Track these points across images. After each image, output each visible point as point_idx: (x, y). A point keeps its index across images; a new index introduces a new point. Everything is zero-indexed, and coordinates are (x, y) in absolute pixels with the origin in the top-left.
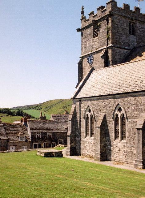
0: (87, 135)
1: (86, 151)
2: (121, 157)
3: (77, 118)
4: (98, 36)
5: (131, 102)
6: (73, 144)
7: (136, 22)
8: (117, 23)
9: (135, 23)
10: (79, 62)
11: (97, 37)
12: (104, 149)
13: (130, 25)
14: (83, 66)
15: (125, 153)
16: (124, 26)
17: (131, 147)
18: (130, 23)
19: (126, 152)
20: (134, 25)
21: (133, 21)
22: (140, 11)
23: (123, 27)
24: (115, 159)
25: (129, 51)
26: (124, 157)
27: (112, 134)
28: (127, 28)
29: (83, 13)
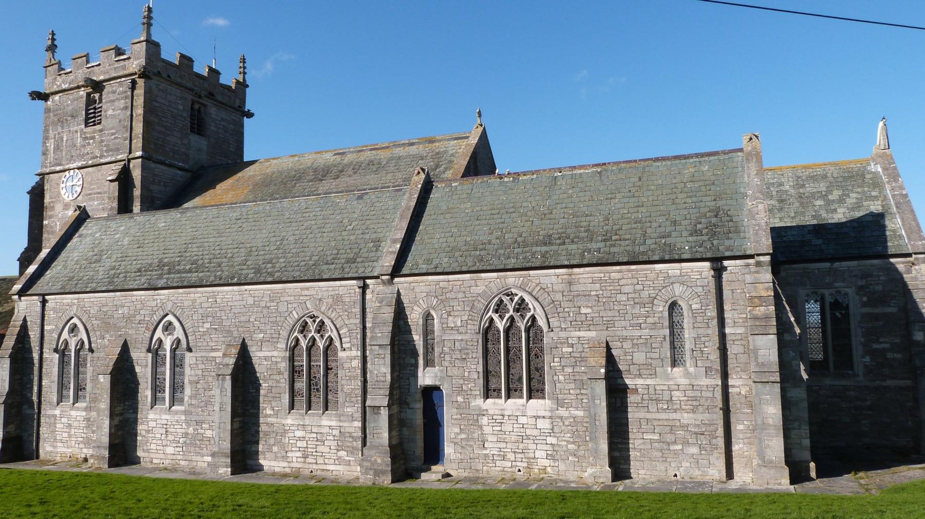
0: (61, 399)
1: (59, 444)
2: (170, 450)
3: (30, 351)
4: (99, 123)
5: (200, 311)
6: (11, 428)
7: (209, 104)
8: (159, 100)
9: (205, 105)
10: (33, 188)
11: (98, 127)
12: (120, 433)
13: (192, 109)
14: (47, 200)
15: (182, 440)
16: (178, 109)
17: (199, 423)
18: (193, 104)
19: (186, 435)
20: (202, 109)
21: (201, 101)
22: (192, 67)
23: (175, 111)
24: (152, 456)
25: (189, 174)
26: (178, 449)
27: (145, 392)
28: (185, 114)
29: (52, 48)
